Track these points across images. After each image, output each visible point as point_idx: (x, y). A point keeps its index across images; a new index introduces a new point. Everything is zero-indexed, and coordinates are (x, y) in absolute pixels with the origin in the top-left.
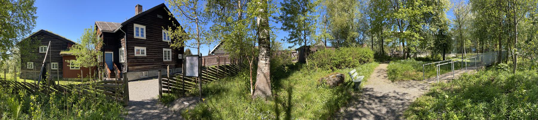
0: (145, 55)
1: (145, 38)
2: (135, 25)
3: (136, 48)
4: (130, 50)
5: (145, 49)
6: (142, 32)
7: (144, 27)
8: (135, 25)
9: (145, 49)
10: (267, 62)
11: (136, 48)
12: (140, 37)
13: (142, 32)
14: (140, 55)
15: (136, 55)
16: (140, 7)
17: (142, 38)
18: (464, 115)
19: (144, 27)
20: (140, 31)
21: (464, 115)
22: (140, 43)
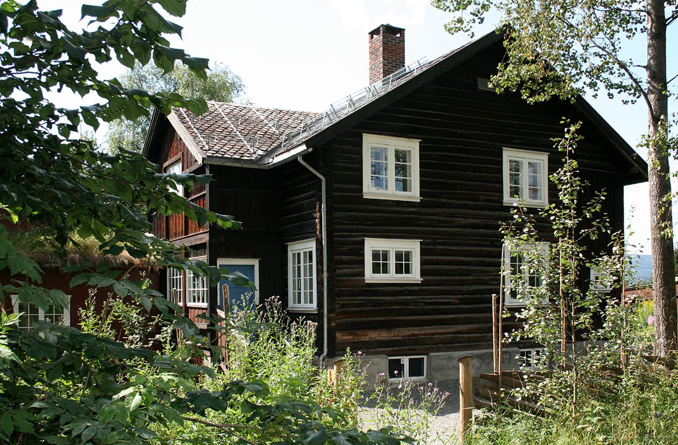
0: (415, 276)
1: (414, 194)
2: (370, 142)
3: (371, 245)
4: (342, 256)
5: (413, 247)
6: (402, 170)
7: (413, 147)
8: (370, 142)
9: (413, 247)
10: (652, 150)
11: (371, 245)
12: (391, 192)
13: (402, 170)
14: (391, 277)
15: (370, 276)
16: (391, 40)
17: (403, 278)
18: (541, 79)
19: (413, 147)
20: (391, 170)
21: (541, 79)
22: (391, 219)
